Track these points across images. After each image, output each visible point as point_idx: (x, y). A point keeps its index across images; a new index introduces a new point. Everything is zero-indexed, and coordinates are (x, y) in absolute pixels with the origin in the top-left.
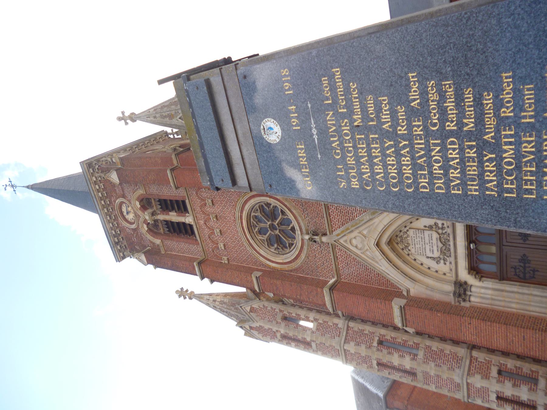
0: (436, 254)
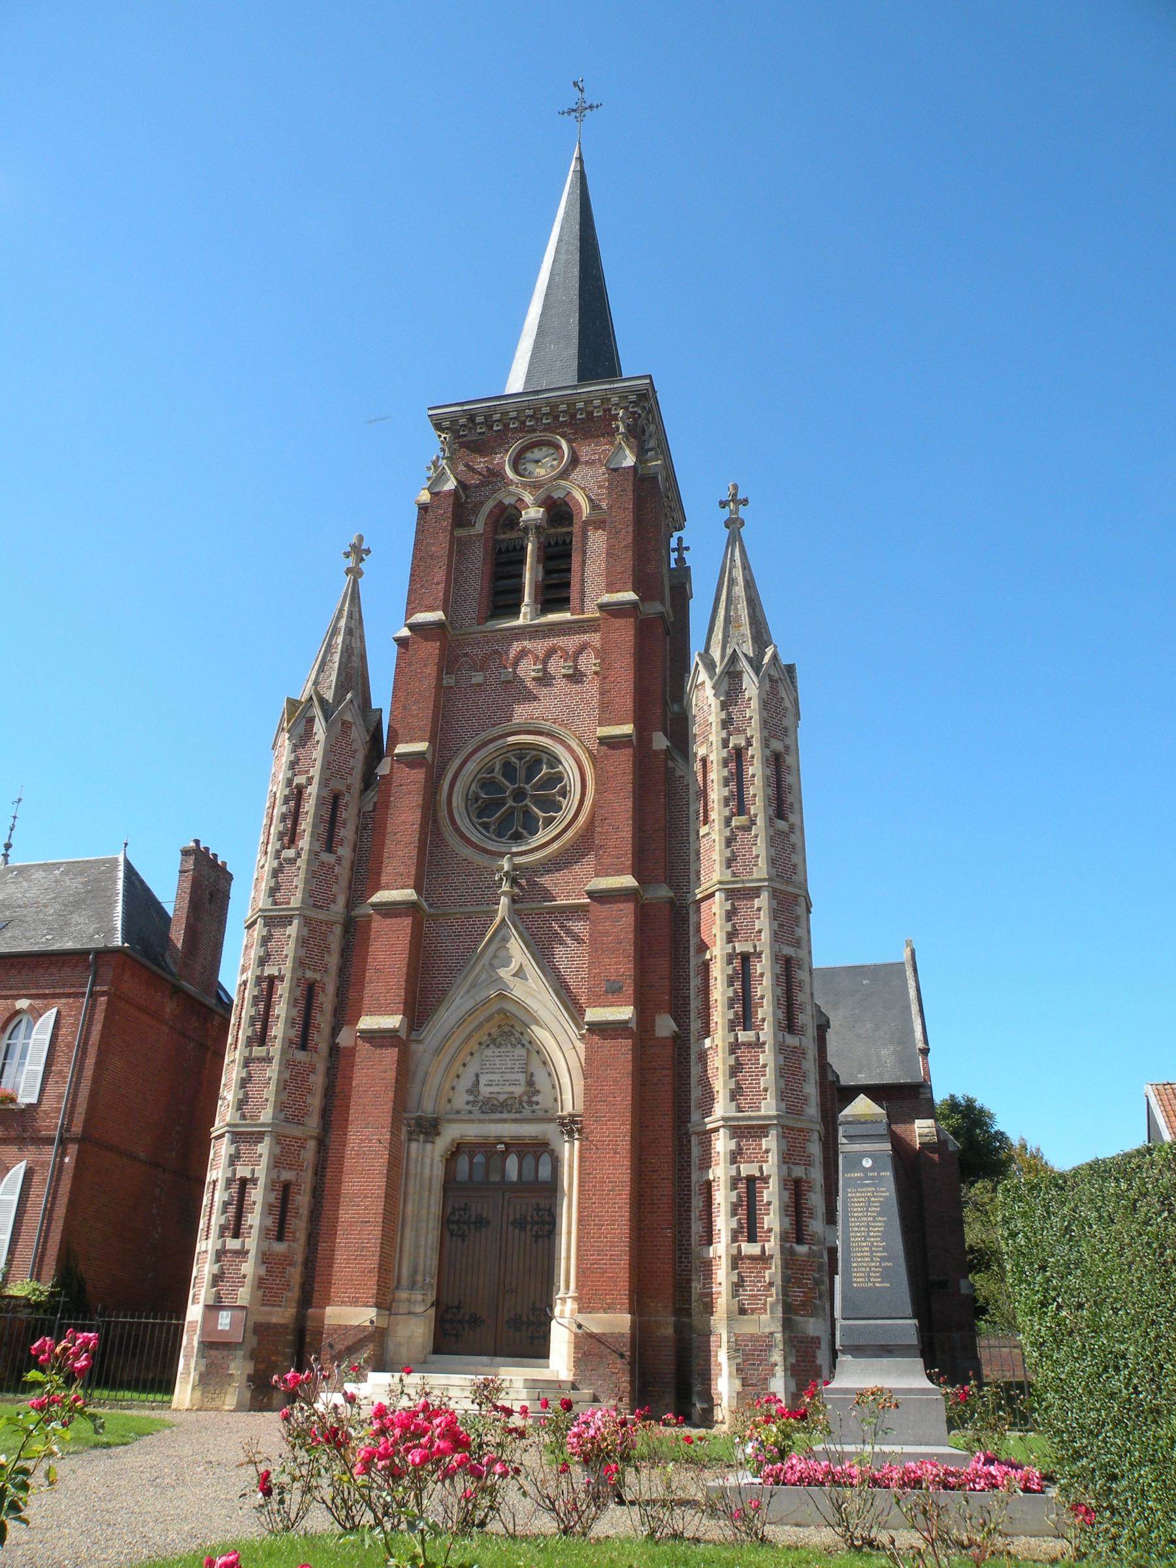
0: (484, 1091)
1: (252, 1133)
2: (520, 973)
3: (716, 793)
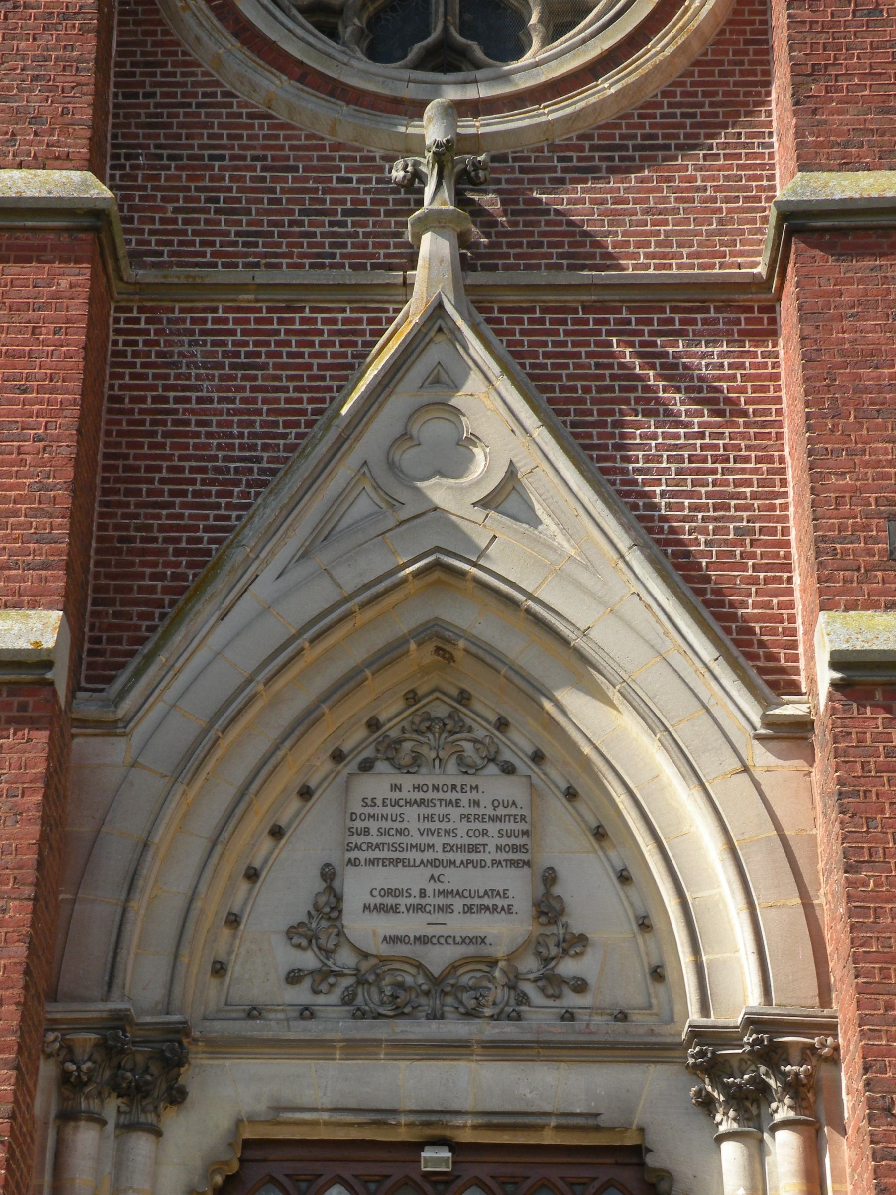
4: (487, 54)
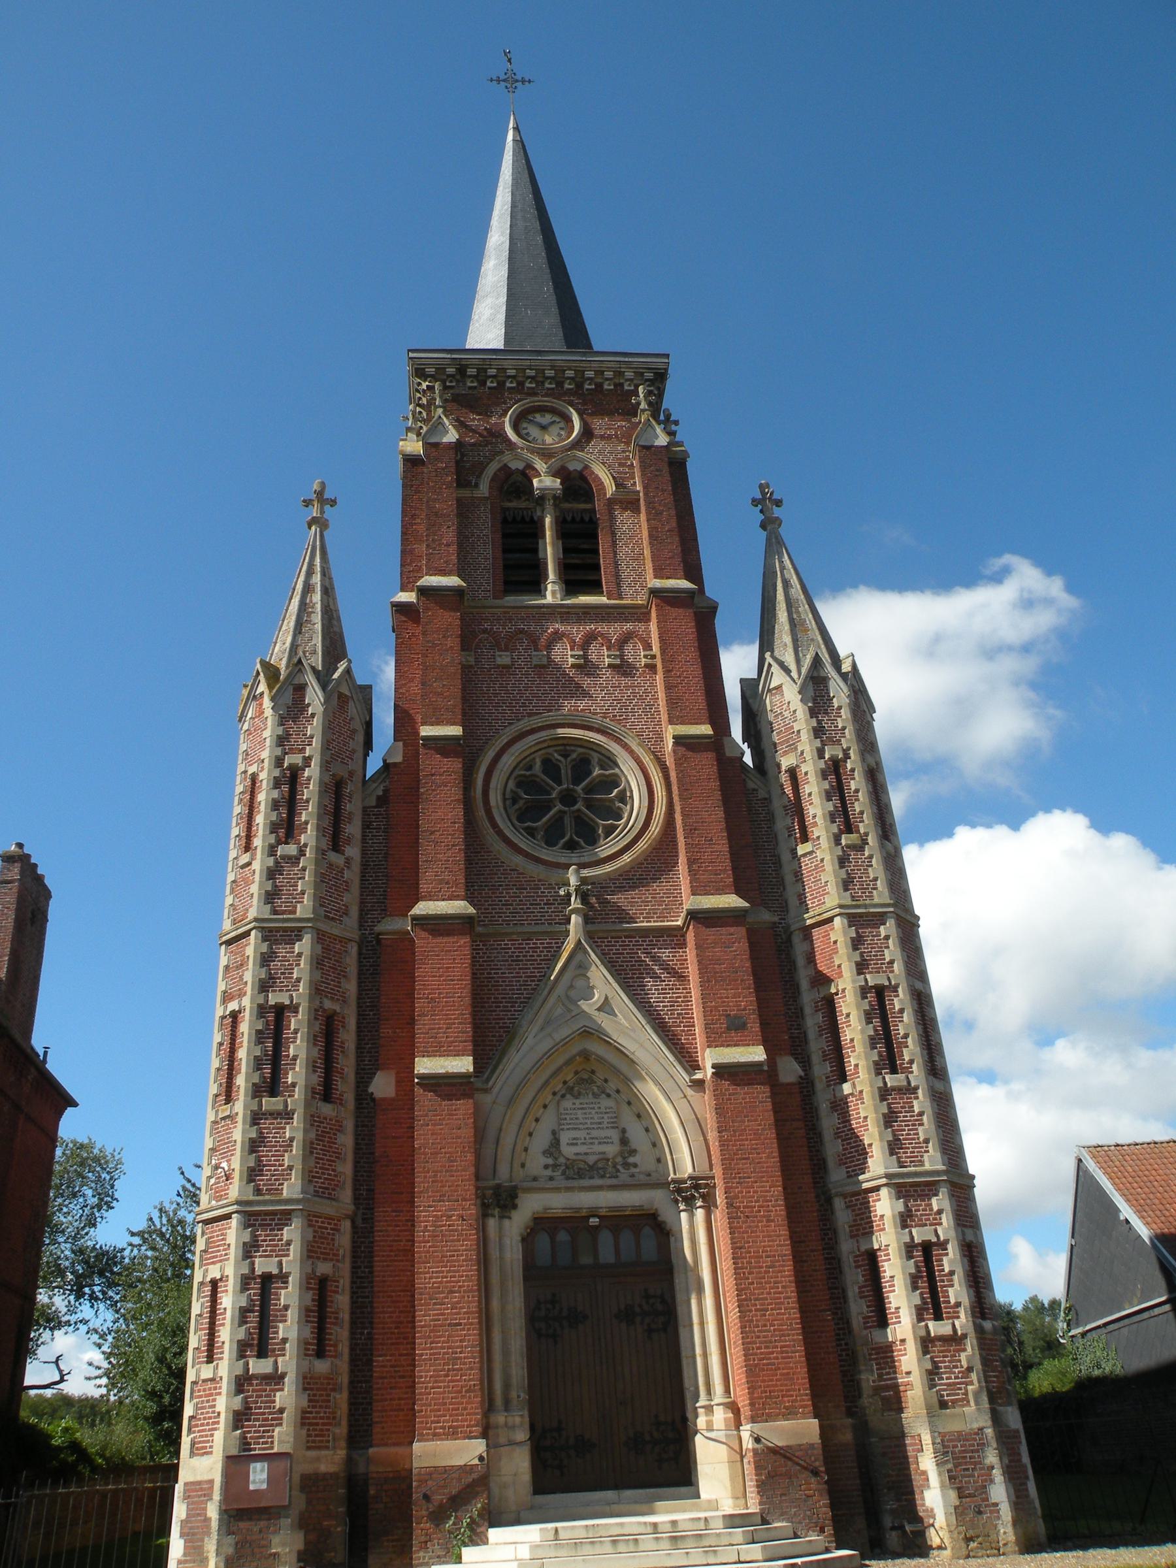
0: (568, 1151)
1: (274, 1213)
2: (606, 1007)
3: (816, 808)
4: (585, 843)
